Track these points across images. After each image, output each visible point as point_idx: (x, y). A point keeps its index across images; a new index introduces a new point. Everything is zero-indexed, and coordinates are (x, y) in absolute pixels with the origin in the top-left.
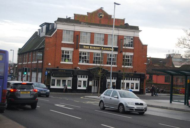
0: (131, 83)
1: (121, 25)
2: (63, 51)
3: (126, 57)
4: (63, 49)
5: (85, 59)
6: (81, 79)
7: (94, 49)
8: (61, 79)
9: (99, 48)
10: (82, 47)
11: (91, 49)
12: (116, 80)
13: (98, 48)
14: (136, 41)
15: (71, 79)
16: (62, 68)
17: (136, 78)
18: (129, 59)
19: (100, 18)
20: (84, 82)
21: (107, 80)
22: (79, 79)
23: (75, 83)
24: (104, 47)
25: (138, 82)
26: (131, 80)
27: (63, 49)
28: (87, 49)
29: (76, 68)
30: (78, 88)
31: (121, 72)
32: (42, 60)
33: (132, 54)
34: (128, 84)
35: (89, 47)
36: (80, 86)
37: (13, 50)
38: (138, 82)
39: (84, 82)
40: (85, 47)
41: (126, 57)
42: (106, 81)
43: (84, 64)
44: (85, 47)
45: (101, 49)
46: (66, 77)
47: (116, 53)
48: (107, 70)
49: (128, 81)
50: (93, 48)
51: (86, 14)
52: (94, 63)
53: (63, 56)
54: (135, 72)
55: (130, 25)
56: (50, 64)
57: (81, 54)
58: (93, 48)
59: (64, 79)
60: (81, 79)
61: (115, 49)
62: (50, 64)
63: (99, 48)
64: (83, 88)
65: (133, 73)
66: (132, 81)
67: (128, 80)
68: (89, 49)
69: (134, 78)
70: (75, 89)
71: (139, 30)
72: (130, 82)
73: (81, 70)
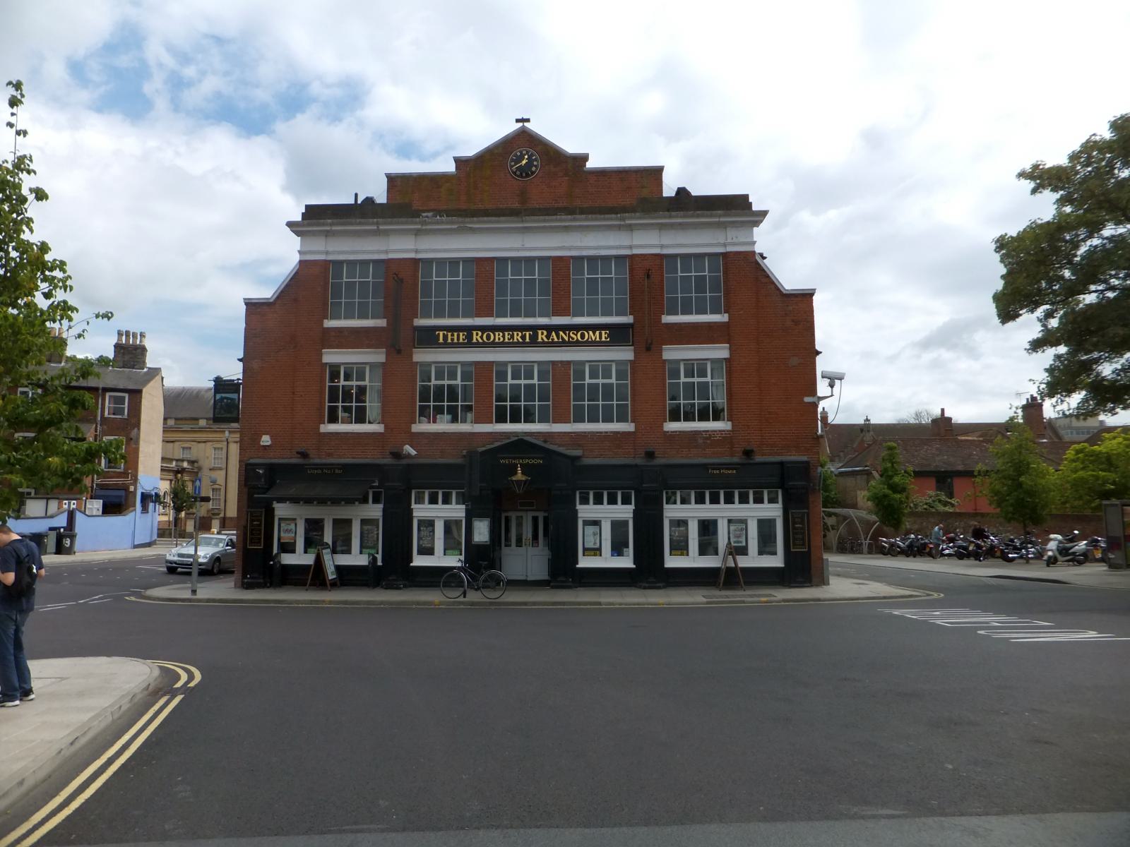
0: (730, 521)
1: (636, 191)
2: (334, 371)
3: (689, 373)
4: (331, 357)
5: (444, 400)
6: (436, 512)
7: (494, 345)
8: (328, 515)
9: (523, 337)
10: (428, 338)
11: (478, 345)
12: (631, 507)
13: (517, 337)
14: (747, 273)
15: (375, 511)
16: (330, 455)
17: (758, 487)
18: (366, 383)
19: (523, 175)
20: (449, 526)
21: (579, 507)
22: (421, 511)
23: (398, 533)
24: (550, 329)
25: (773, 511)
26: (729, 500)
27: (331, 357)
28: (459, 345)
29: (397, 455)
30: (419, 561)
31: (660, 461)
32: (197, 419)
33: (720, 352)
34: (708, 528)
35: (469, 337)
36: (429, 551)
37: (832, 396)
38: (773, 511)
39: (449, 526)
40: (445, 337)
41: (689, 373)
42: (410, 518)
43: (443, 425)
44: (445, 337)
45: (534, 338)
46: (350, 501)
47: (625, 354)
48: (577, 452)
49: (708, 511)
50: (488, 337)
51: (451, 168)
52: (501, 419)
53: (425, 396)
54: (748, 453)
55: (696, 191)
56: (266, 440)
57: (335, 375)
58: (488, 337)
59: (343, 512)
60: (436, 512)
61: (618, 335)
62: (266, 440)
63: (523, 337)
64: (443, 559)
65: (735, 460)
66: (737, 510)
67: (737, 505)
68: (469, 344)
69: (744, 486)
70: (393, 569)
71: (754, 208)
72: (720, 512)
73: (421, 461)
